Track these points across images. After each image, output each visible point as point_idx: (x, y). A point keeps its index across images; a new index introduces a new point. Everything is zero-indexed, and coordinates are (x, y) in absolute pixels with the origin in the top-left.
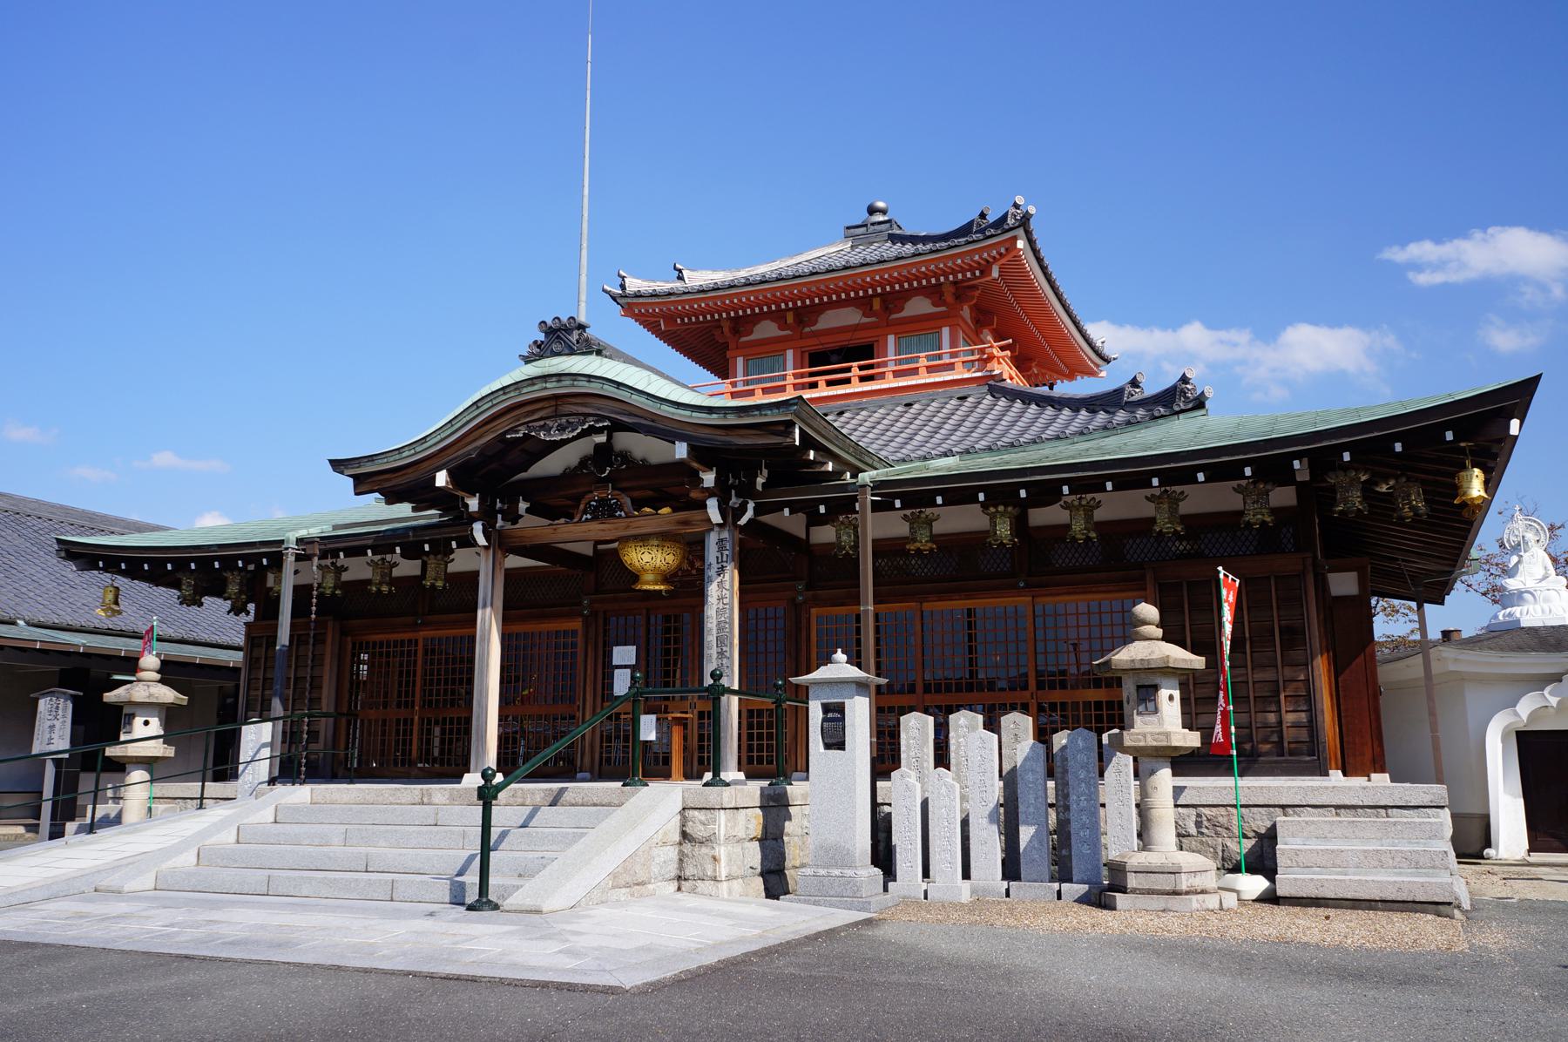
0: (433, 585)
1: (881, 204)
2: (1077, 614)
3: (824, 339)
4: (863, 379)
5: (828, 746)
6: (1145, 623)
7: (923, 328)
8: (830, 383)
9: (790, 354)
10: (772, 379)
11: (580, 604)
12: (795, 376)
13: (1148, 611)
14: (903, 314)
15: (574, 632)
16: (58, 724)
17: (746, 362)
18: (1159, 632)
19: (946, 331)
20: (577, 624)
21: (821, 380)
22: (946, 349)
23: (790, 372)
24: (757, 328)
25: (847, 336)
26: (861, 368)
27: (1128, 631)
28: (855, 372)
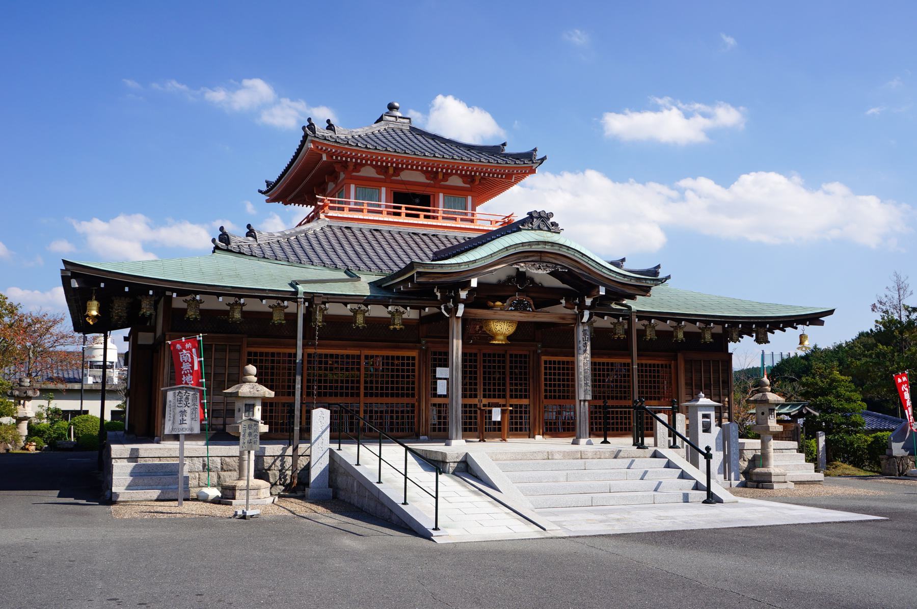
0: (714, 335)
1: (397, 104)
2: (104, 367)
3: (408, 187)
4: (407, 215)
5: (704, 431)
6: (251, 375)
7: (367, 184)
8: (426, 217)
9: (384, 190)
10: (339, 202)
11: (419, 342)
12: (444, 212)
13: (252, 369)
14: (399, 178)
15: (413, 358)
16: (188, 410)
17: (356, 188)
18: (255, 379)
19: (470, 198)
20: (414, 353)
21: (422, 214)
22: (469, 211)
23: (383, 203)
24: (363, 169)
25: (423, 189)
26: (407, 209)
27: (240, 378)
28: (403, 211)
